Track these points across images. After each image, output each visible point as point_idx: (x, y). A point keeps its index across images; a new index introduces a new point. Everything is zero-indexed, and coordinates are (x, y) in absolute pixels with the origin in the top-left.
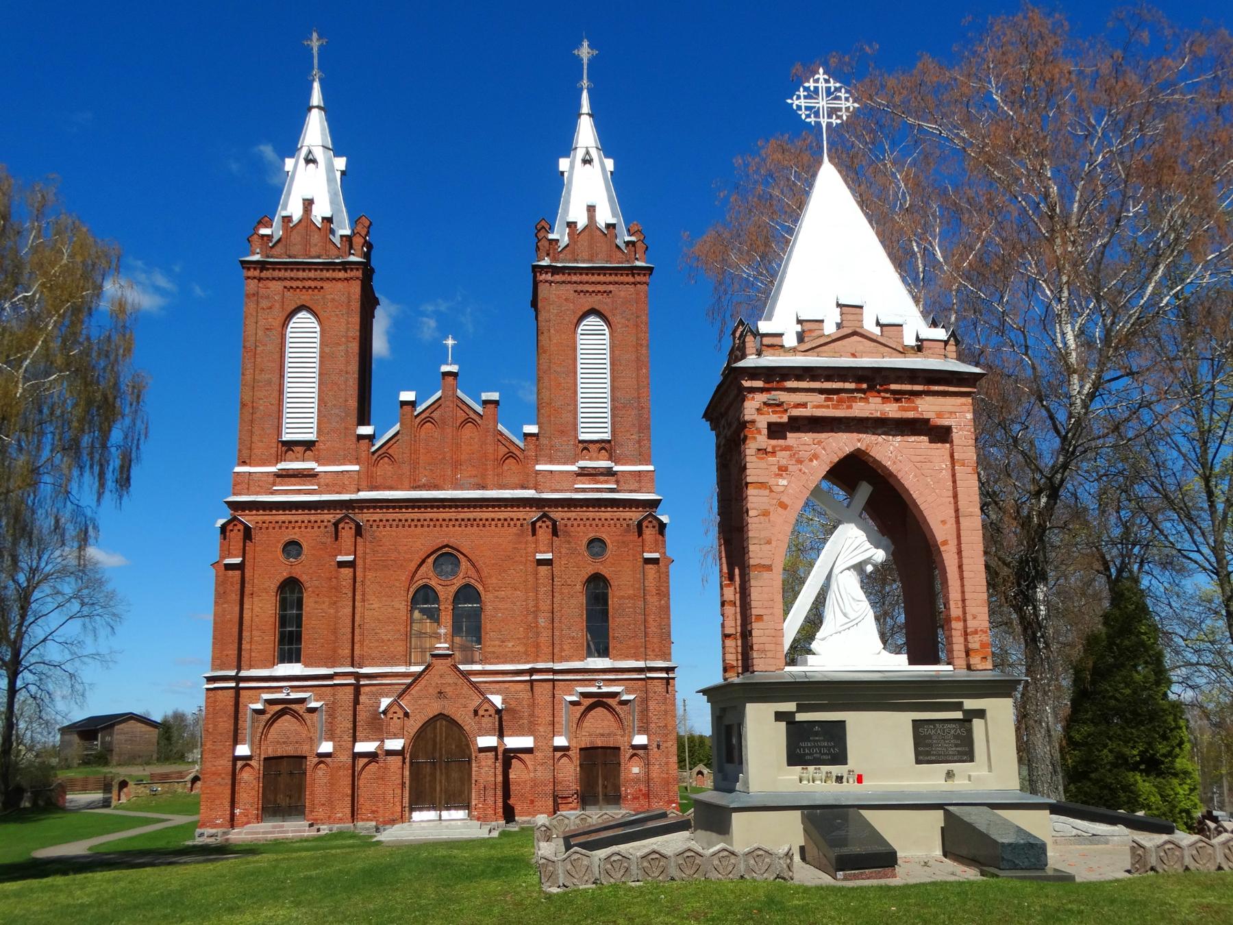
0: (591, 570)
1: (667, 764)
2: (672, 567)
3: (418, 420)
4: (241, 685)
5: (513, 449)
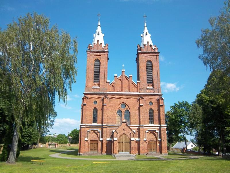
0: (150, 108)
1: (165, 144)
2: (165, 107)
3: (118, 79)
4: (82, 127)
5: (135, 85)
